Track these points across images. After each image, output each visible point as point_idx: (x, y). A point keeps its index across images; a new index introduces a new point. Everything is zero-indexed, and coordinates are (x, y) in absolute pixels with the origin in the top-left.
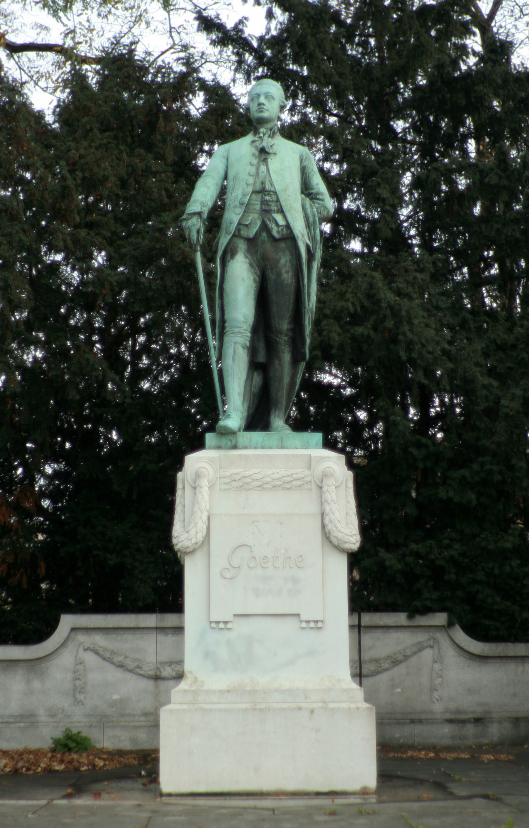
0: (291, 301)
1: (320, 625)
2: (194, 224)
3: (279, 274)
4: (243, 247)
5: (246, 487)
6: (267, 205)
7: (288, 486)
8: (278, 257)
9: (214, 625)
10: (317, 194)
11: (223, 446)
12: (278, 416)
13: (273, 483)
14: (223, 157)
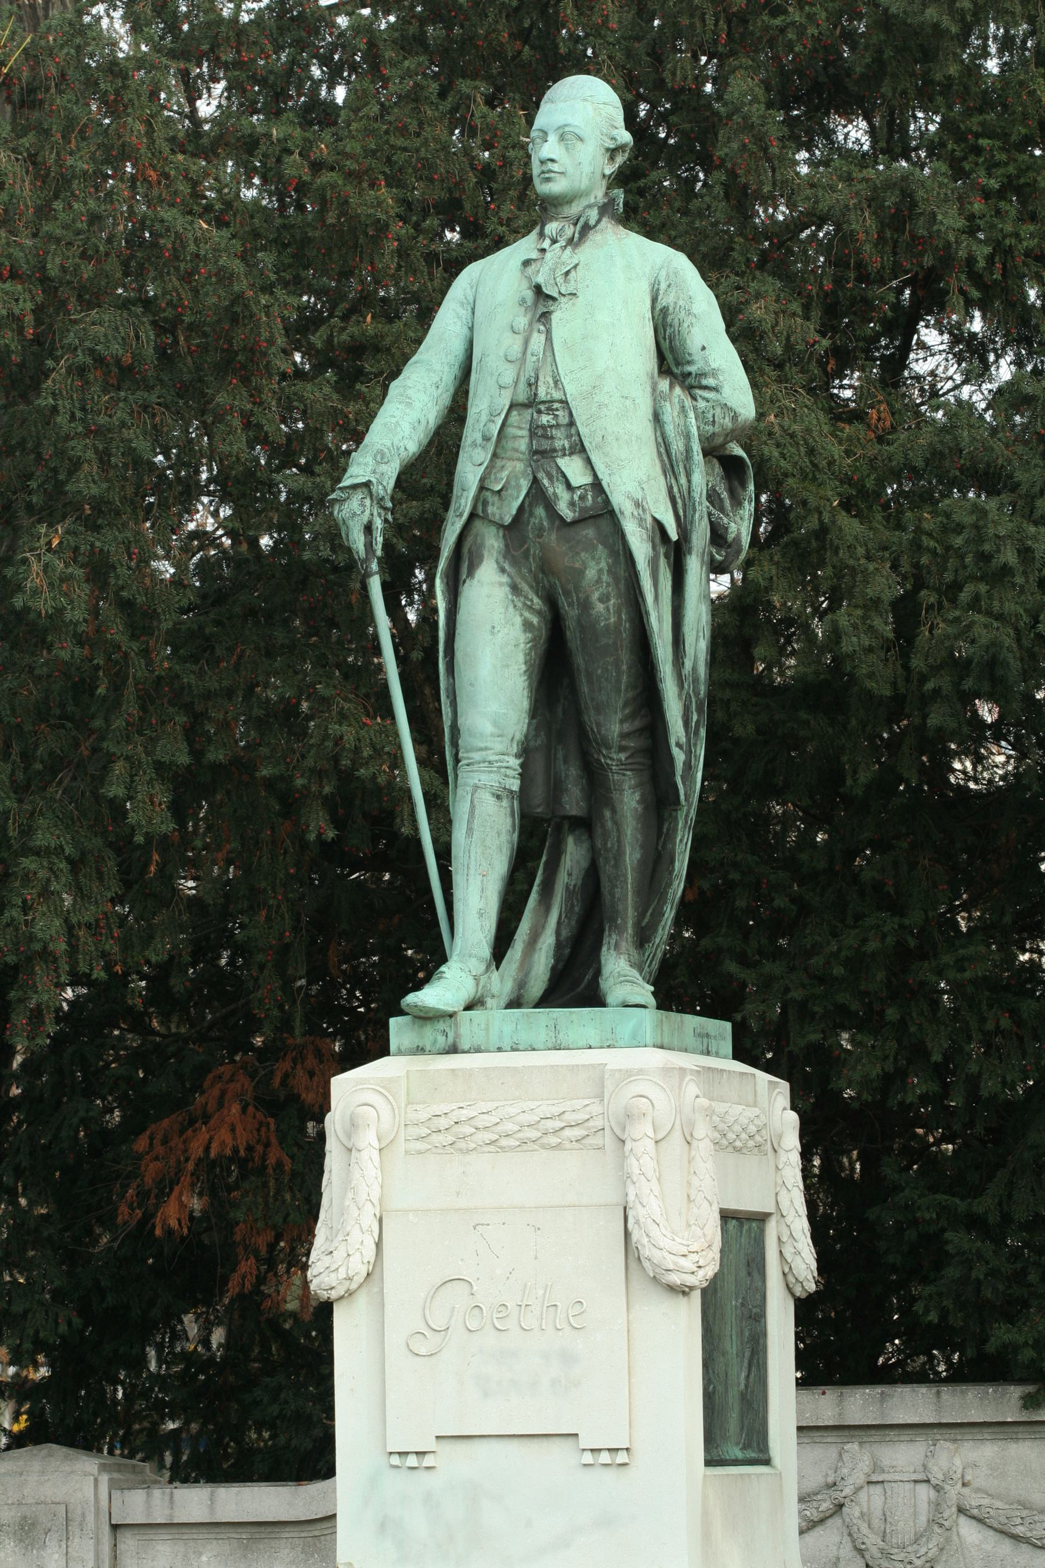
0: (624, 667)
1: (622, 1457)
2: (354, 514)
3: (585, 605)
4: (496, 545)
5: (462, 1145)
6: (545, 437)
7: (553, 1140)
8: (577, 565)
9: (395, 1460)
10: (703, 375)
11: (428, 1048)
12: (617, 946)
13: (520, 1135)
14: (462, 304)
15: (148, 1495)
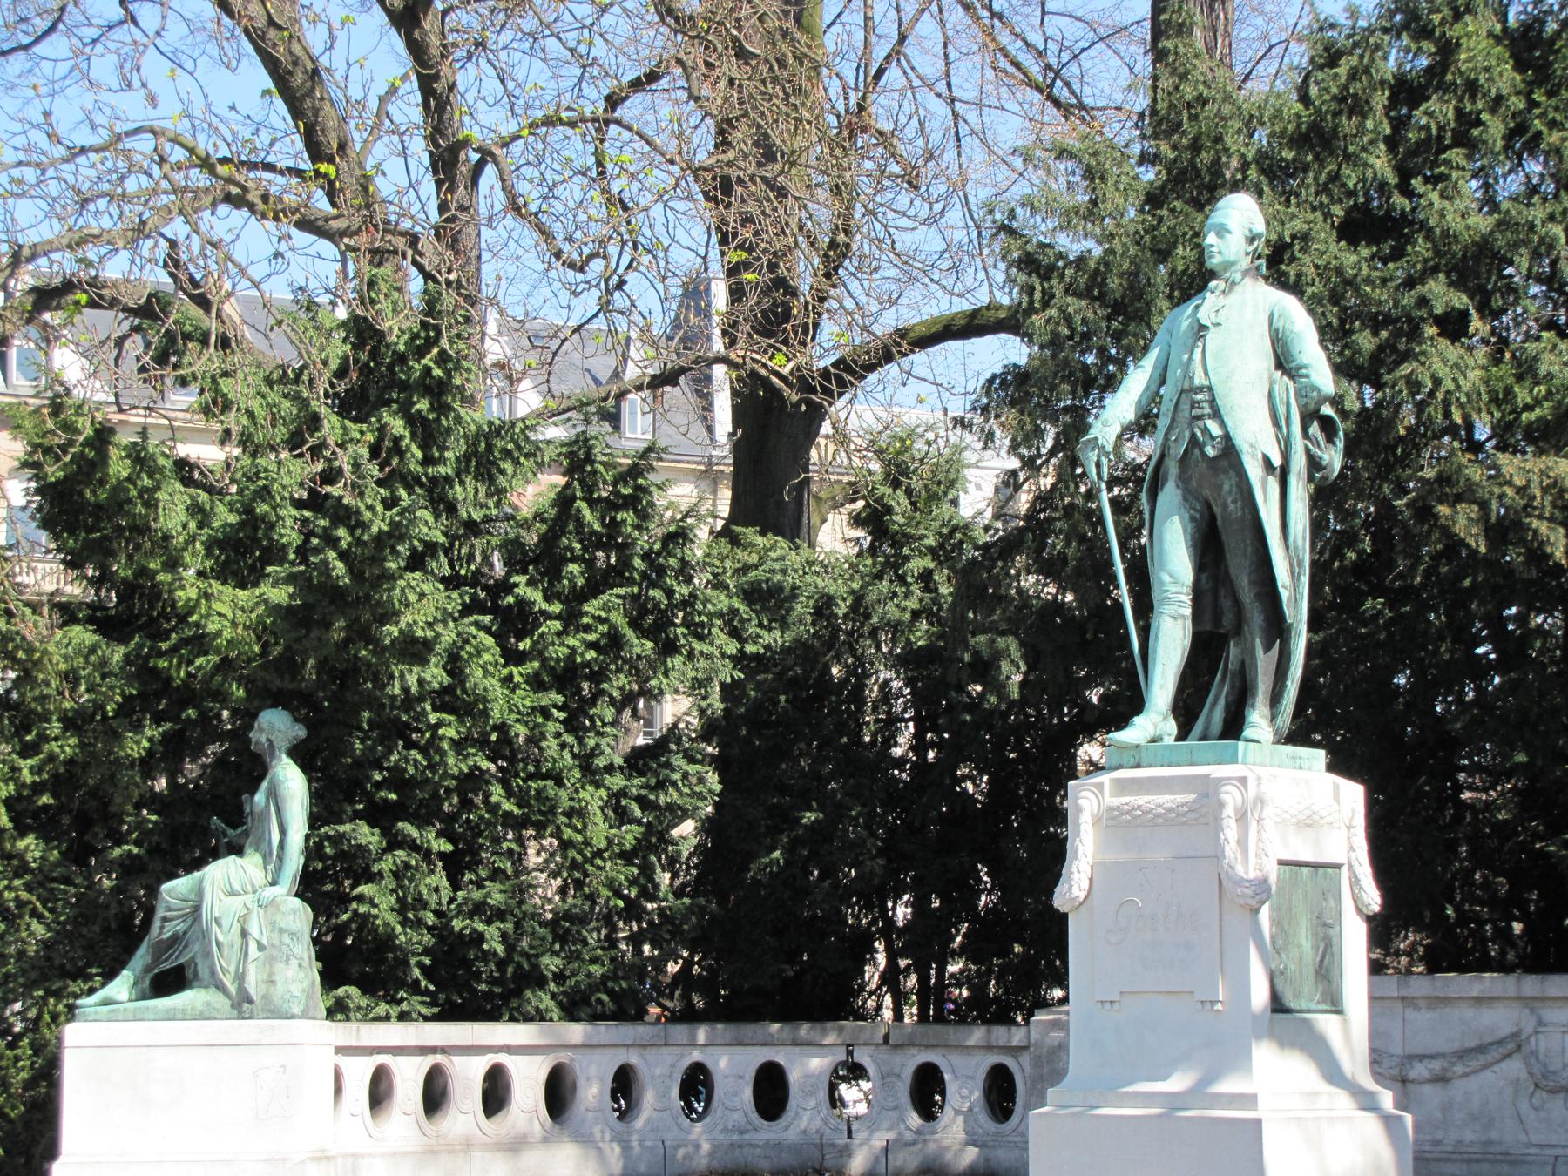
15: (989, 1032)
